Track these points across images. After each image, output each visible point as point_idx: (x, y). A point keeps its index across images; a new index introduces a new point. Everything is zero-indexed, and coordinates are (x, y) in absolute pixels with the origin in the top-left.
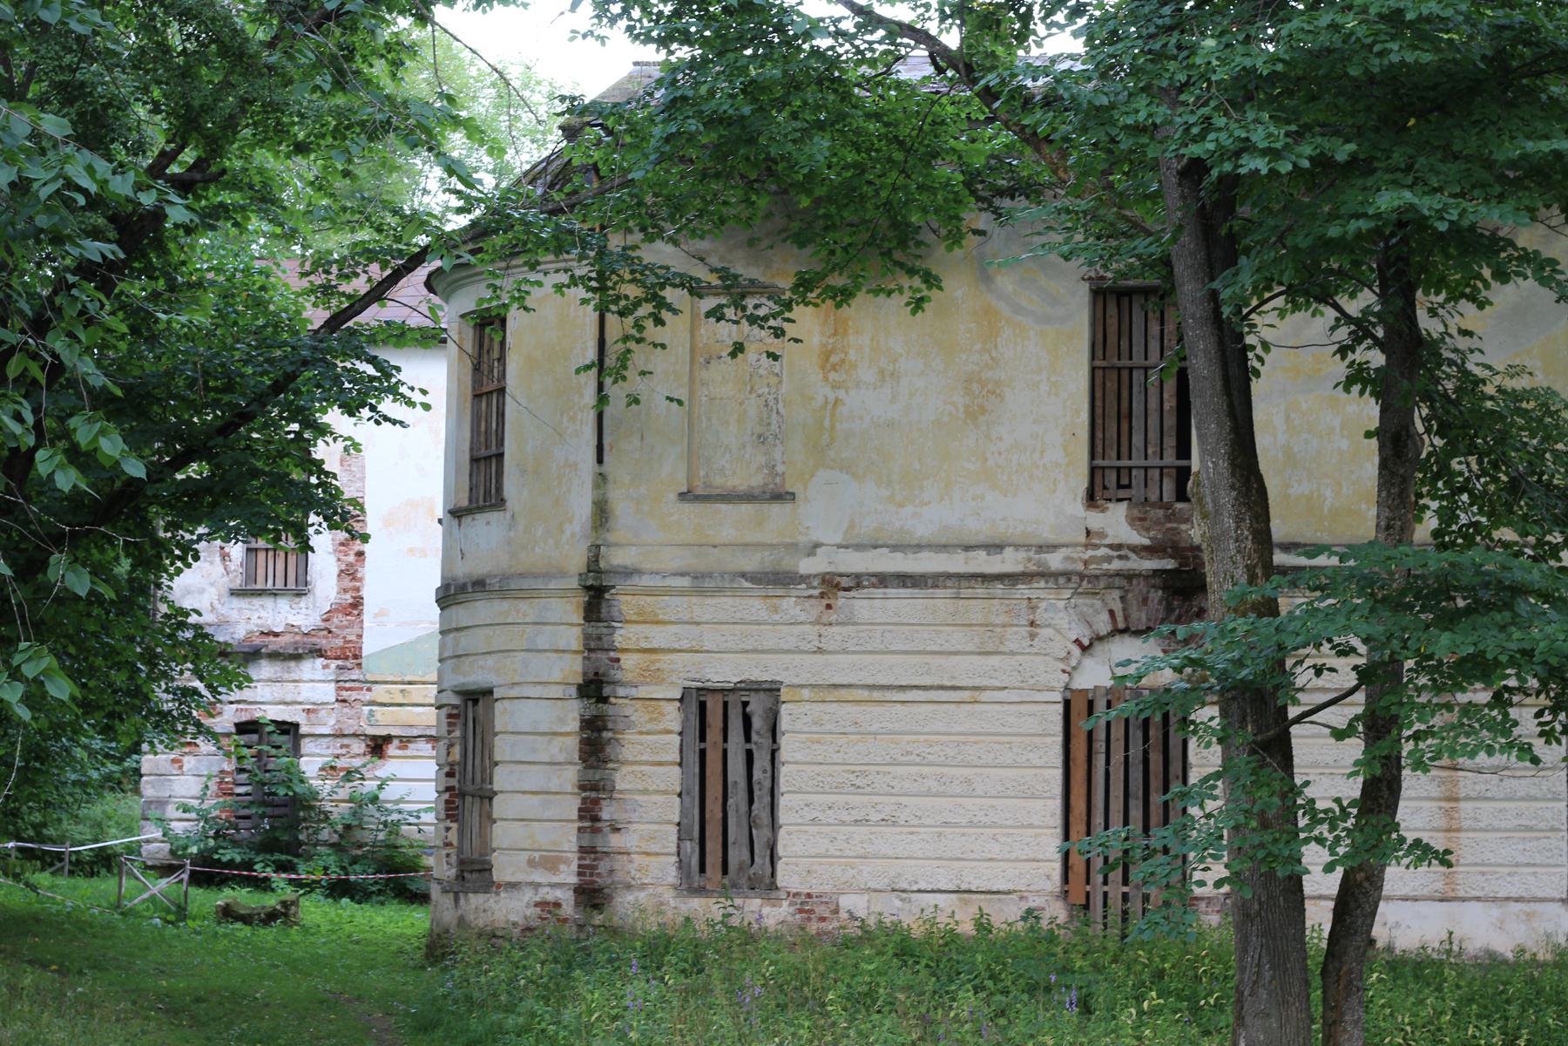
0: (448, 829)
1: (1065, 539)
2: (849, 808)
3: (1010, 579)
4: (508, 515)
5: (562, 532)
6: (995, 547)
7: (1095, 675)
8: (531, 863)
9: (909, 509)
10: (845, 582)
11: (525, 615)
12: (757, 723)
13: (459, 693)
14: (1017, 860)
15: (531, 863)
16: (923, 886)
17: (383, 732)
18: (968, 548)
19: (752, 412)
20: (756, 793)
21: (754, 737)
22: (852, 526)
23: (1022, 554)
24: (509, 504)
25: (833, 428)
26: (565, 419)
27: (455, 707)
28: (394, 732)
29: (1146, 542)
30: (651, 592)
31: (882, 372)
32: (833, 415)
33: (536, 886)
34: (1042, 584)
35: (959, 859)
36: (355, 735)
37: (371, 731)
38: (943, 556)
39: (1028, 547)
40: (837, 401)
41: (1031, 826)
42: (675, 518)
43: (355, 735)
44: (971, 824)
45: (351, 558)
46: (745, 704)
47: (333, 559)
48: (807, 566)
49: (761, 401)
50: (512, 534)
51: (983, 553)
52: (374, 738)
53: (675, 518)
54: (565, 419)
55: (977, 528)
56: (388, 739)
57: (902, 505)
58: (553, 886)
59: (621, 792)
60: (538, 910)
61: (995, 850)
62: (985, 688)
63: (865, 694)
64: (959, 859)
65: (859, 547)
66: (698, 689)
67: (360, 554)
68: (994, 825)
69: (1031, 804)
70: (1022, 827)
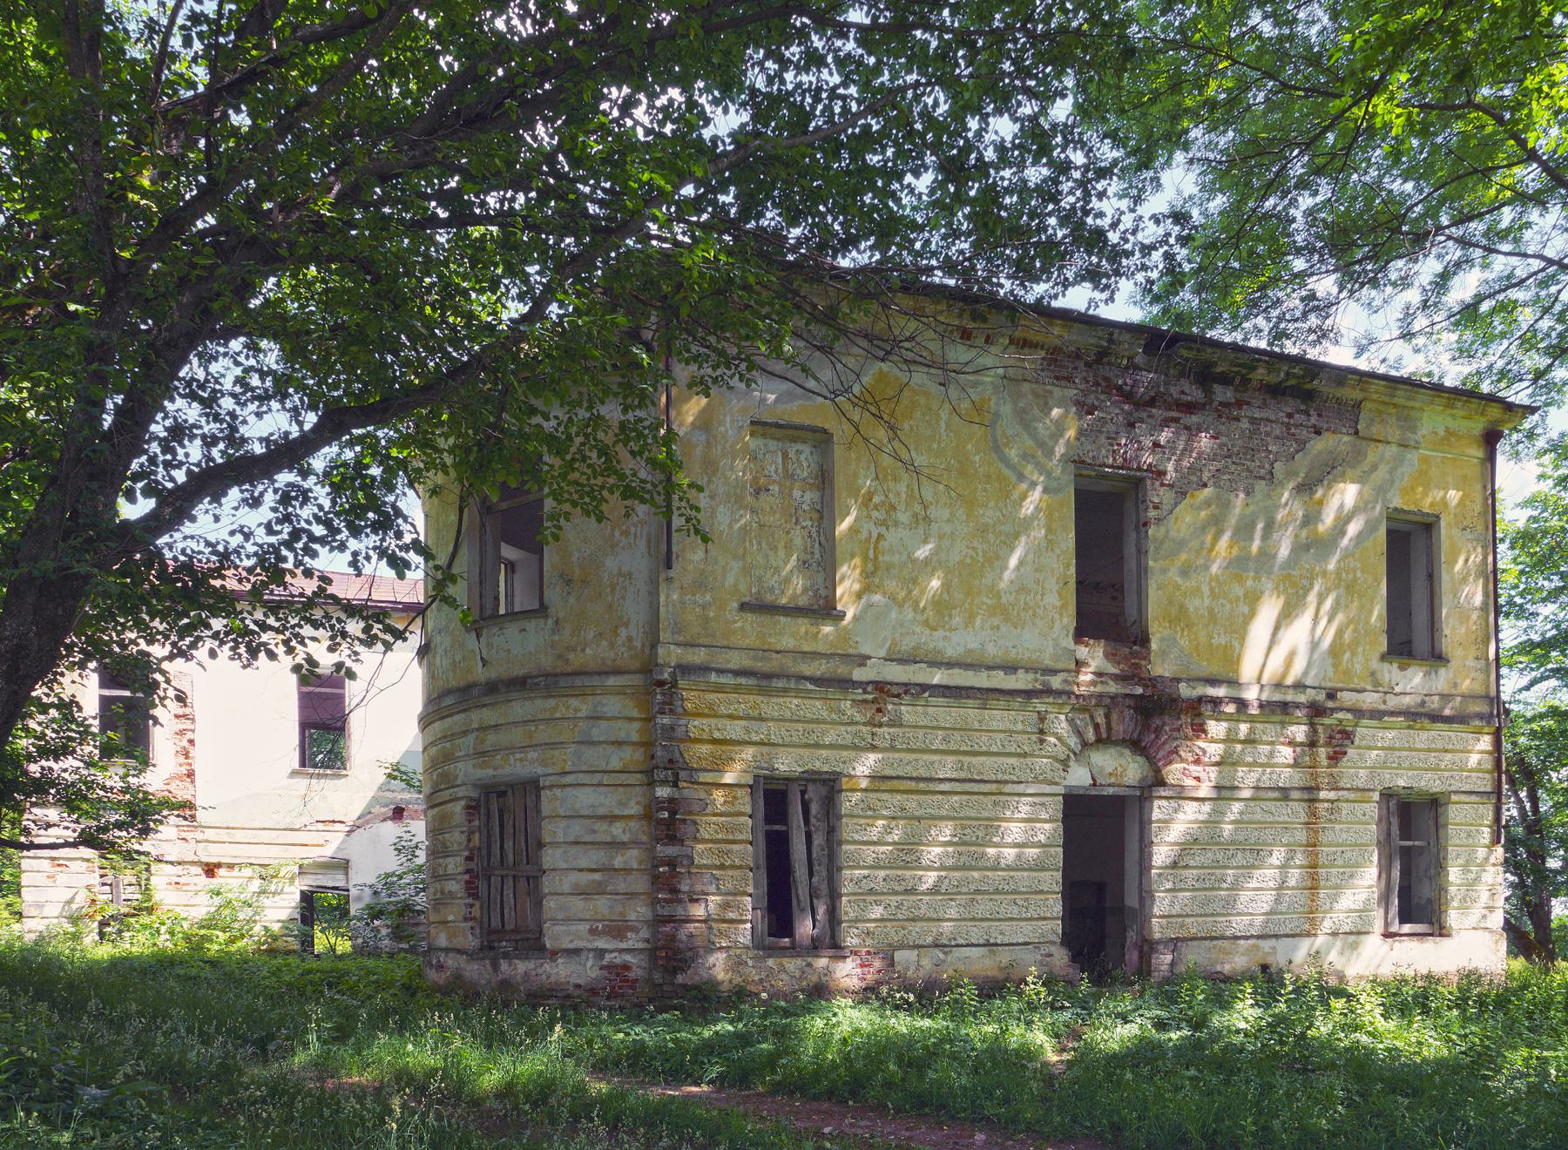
0: (472, 906)
1: (1060, 666)
2: (900, 880)
3: (1028, 694)
4: (550, 621)
5: (618, 635)
6: (1010, 668)
7: (1079, 777)
8: (593, 932)
9: (940, 633)
10: (895, 690)
11: (576, 710)
12: (814, 808)
13: (475, 786)
14: (1031, 919)
15: (593, 932)
16: (961, 941)
17: (215, 860)
18: (989, 668)
19: (798, 541)
20: (816, 868)
21: (813, 820)
22: (894, 643)
23: (1031, 676)
24: (552, 611)
25: (876, 558)
26: (617, 533)
27: (472, 799)
28: (224, 860)
29: (1116, 671)
30: (719, 689)
31: (916, 515)
32: (876, 548)
33: (601, 953)
34: (1051, 700)
35: (988, 919)
36: (193, 863)
37: (205, 859)
38: (971, 673)
39: (1035, 671)
40: (880, 536)
41: (1041, 892)
42: (739, 624)
43: (193, 863)
44: (997, 892)
45: (185, 743)
46: (803, 793)
47: (170, 743)
48: (859, 674)
49: (805, 534)
50: (556, 638)
51: (1001, 673)
52: (207, 864)
53: (739, 624)
54: (617, 533)
55: (993, 651)
56: (219, 865)
57: (935, 629)
58: (621, 951)
59: (698, 867)
60: (605, 973)
61: (1014, 911)
62: (1006, 782)
63: (912, 785)
64: (988, 919)
65: (902, 661)
66: (766, 777)
67: (191, 742)
68: (1014, 892)
69: (1041, 874)
70: (1036, 893)
